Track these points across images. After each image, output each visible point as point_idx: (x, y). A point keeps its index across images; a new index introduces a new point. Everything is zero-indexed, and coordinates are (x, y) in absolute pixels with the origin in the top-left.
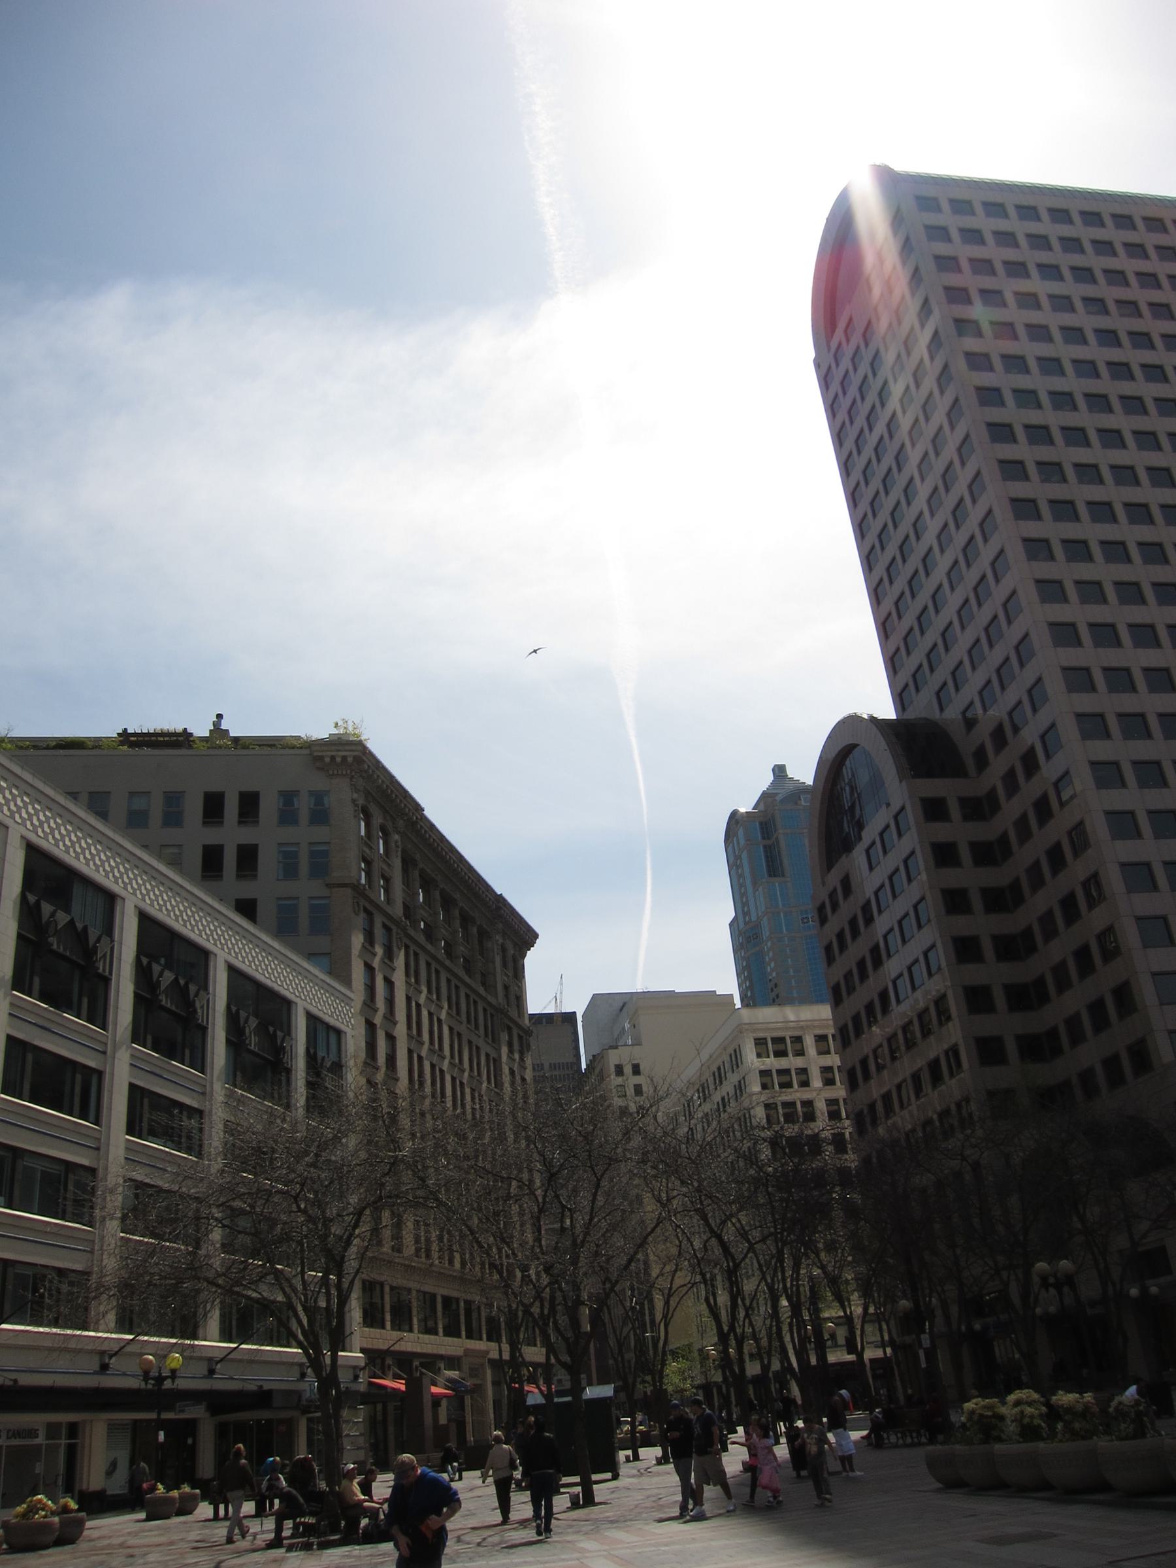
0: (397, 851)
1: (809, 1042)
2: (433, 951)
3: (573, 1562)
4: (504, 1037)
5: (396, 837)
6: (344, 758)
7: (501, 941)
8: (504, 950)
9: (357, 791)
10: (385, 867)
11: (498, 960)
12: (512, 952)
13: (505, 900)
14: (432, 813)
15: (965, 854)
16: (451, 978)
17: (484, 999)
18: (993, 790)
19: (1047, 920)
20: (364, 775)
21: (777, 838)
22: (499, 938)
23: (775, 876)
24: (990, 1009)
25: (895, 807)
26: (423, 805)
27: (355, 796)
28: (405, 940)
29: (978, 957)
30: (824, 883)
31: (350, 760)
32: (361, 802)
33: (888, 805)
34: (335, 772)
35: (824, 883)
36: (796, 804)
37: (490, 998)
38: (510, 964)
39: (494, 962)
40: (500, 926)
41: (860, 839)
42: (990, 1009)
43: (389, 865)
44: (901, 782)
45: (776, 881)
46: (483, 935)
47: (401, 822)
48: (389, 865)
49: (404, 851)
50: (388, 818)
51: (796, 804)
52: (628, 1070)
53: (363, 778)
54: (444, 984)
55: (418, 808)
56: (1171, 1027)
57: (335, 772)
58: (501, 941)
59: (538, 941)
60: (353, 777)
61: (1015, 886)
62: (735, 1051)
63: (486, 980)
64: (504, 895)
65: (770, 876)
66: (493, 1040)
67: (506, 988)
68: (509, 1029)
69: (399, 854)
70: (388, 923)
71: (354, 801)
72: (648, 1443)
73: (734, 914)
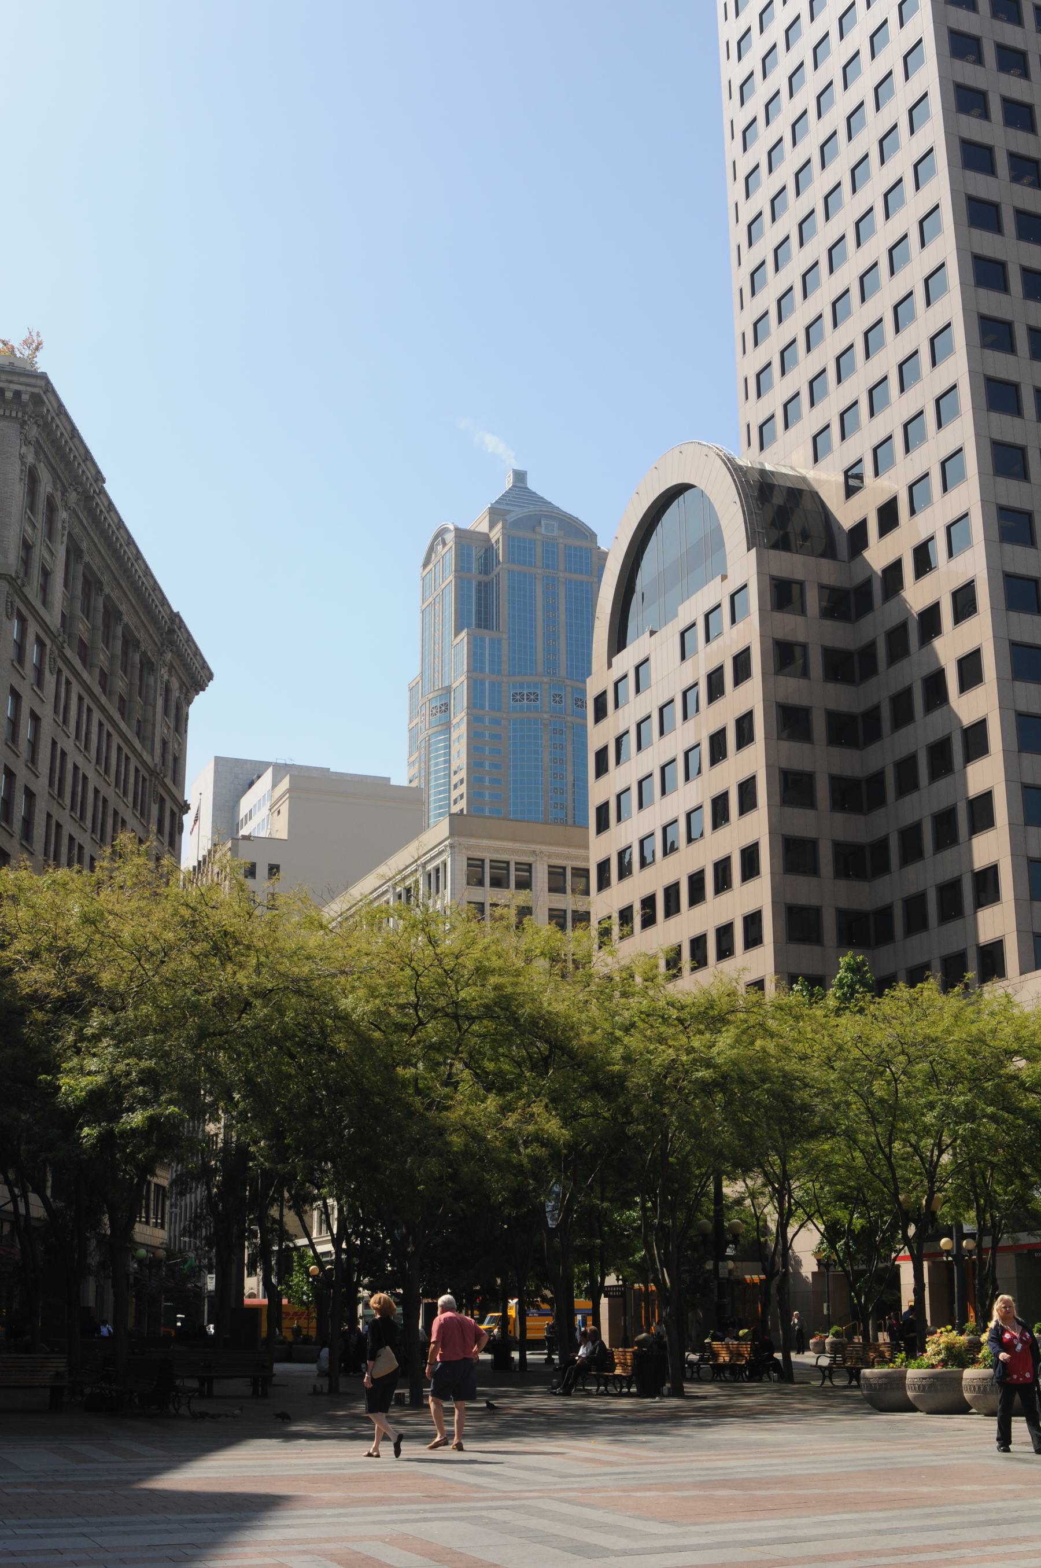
0: (63, 535)
1: (541, 877)
2: (88, 682)
3: (575, 1494)
4: (155, 809)
5: (64, 515)
6: (17, 394)
7: (166, 677)
8: (168, 690)
9: (27, 442)
10: (47, 556)
11: (160, 702)
12: (177, 695)
13: (181, 621)
14: (114, 489)
15: (819, 727)
16: (105, 721)
17: (138, 756)
18: (873, 645)
19: (906, 767)
20: (41, 422)
21: (498, 576)
22: (164, 672)
23: (486, 627)
24: (813, 870)
25: (732, 585)
26: (105, 474)
27: (24, 450)
28: (60, 663)
29: (809, 802)
30: (610, 665)
31: (25, 397)
32: (30, 459)
33: (724, 578)
34: (7, 413)
35: (610, 665)
36: (534, 530)
37: (146, 756)
38: (173, 712)
39: (154, 707)
40: (169, 656)
41: (676, 615)
42: (813, 870)
43: (52, 554)
44: (749, 550)
45: (487, 635)
46: (148, 666)
47: (74, 494)
48: (52, 554)
49: (70, 534)
50: (59, 486)
51: (534, 530)
52: (262, 871)
53: (39, 426)
54: (95, 729)
55: (99, 478)
56: (1036, 930)
57: (14, 414)
58: (166, 677)
59: (211, 684)
60: (25, 422)
61: (872, 716)
62: (437, 870)
63: (142, 730)
64: (182, 615)
65: (479, 626)
66: (142, 814)
67: (164, 743)
68: (162, 801)
69: (65, 539)
70: (43, 635)
71: (22, 457)
72: (730, 1360)
73: (418, 670)
